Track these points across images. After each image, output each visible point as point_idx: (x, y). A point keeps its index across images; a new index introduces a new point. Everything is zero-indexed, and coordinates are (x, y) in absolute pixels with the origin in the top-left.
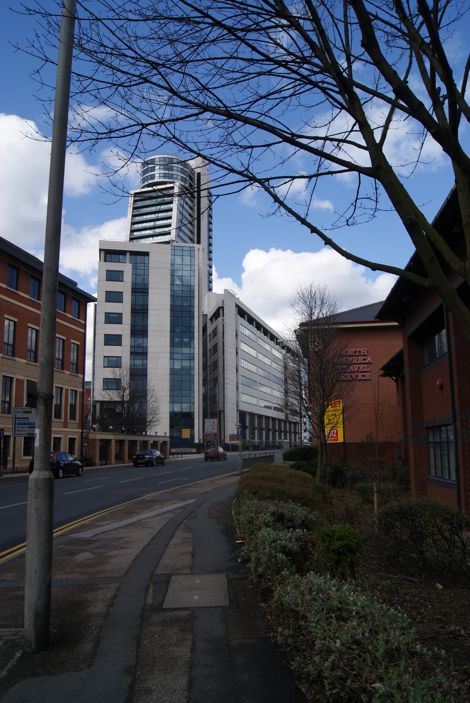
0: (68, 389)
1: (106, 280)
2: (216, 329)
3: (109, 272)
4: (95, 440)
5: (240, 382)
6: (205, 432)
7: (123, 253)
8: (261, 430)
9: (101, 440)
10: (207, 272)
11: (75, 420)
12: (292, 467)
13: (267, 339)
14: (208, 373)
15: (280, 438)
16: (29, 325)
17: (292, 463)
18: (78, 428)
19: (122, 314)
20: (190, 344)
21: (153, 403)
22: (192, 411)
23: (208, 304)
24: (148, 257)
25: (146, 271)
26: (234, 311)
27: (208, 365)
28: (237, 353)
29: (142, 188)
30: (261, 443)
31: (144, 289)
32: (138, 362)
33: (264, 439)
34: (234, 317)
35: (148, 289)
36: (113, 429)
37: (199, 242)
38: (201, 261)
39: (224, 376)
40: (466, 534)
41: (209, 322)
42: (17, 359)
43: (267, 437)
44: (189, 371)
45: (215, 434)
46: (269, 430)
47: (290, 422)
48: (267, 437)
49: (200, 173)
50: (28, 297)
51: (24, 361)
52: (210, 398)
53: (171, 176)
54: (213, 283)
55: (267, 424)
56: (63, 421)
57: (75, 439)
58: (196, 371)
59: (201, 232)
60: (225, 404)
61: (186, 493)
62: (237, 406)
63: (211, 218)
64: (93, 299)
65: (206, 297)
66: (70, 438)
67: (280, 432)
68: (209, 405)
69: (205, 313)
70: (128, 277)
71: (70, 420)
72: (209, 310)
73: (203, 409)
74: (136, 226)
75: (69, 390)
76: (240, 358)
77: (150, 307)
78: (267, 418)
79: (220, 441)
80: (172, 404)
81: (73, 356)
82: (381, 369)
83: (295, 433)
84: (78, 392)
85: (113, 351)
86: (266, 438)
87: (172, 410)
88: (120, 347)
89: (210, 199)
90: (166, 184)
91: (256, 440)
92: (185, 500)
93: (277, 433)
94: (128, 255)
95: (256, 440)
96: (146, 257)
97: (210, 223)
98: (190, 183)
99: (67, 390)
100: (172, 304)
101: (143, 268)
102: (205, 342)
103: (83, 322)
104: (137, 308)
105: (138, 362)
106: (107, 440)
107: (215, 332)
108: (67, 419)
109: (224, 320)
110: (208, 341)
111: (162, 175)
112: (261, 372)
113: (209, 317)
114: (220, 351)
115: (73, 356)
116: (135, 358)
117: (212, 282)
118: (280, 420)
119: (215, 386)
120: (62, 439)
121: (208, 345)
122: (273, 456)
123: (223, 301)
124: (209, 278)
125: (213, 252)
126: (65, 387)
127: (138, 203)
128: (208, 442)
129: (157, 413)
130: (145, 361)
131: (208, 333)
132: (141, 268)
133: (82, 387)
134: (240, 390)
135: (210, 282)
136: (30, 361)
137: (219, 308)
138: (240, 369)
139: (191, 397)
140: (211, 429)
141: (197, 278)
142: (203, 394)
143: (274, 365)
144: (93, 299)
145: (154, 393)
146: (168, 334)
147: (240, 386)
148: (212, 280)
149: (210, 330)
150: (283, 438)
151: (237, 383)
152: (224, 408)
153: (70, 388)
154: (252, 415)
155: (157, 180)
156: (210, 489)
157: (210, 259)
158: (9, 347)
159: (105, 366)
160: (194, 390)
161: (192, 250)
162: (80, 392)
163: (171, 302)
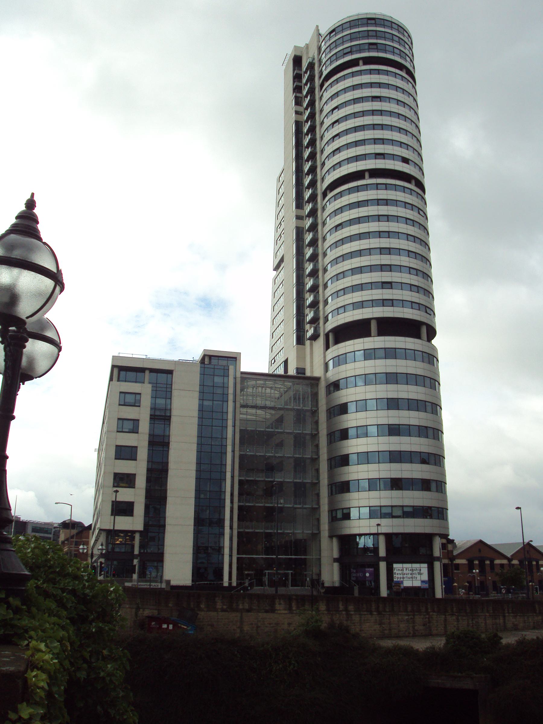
24: (171, 375)
25: (168, 393)
40: (541, 562)
70: (146, 401)
94: (147, 372)
96: (169, 376)
104: (158, 413)
132: (161, 386)
159: (120, 404)
160: (226, 465)
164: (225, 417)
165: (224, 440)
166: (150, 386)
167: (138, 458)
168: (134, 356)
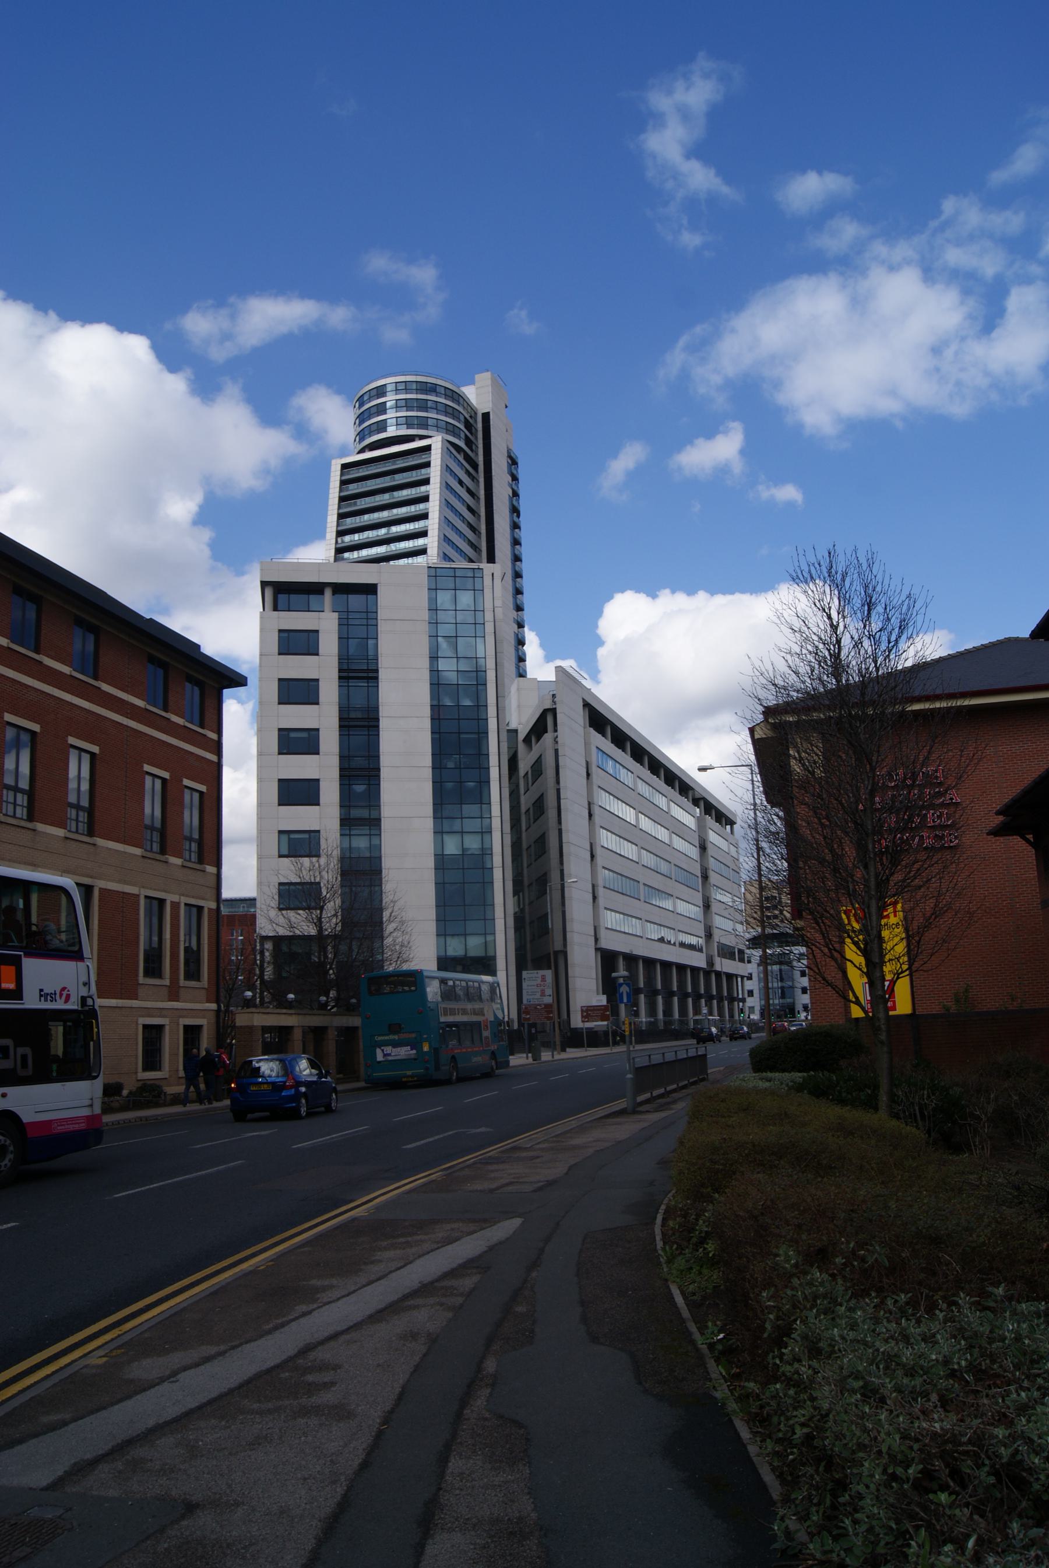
0: (179, 903)
1: (280, 654)
2: (538, 762)
3: (286, 635)
4: (250, 1029)
5: (600, 883)
6: (525, 1001)
7: (315, 589)
8: (652, 994)
9: (265, 1029)
10: (513, 635)
11: (198, 979)
12: (799, 1088)
13: (660, 783)
14: (525, 865)
15: (697, 1011)
16: (72, 740)
17: (798, 1076)
18: (208, 1001)
19: (318, 730)
20: (481, 796)
21: (395, 934)
22: (491, 953)
23: (519, 706)
26: (580, 717)
27: (525, 846)
28: (590, 815)
29: (360, 452)
30: (653, 1024)
31: (368, 671)
32: (361, 843)
33: (660, 1015)
34: (581, 730)
35: (377, 671)
36: (295, 1000)
37: (491, 559)
38: (498, 603)
39: (562, 871)
41: (521, 748)
42: (40, 827)
43: (668, 1012)
44: (480, 861)
45: (548, 1007)
46: (672, 994)
47: (718, 974)
48: (668, 1012)
49: (488, 413)
50: (66, 669)
51: (60, 832)
52: (531, 922)
53: (423, 423)
54: (527, 663)
55: (667, 980)
56: (167, 982)
57: (199, 1028)
58: (497, 860)
59: (496, 547)
60: (569, 935)
61: (487, 1185)
62: (596, 940)
63: (518, 516)
64: (237, 680)
65: (514, 689)
66: (145, 1027)
67: (697, 997)
68: (528, 939)
69: (513, 725)
70: (329, 644)
71: (185, 979)
72: (521, 718)
73: (516, 950)
74: (347, 539)
75: (182, 906)
76: (597, 828)
77: (383, 712)
78: (666, 965)
79: (559, 1023)
80: (442, 939)
81: (190, 818)
82: (998, 813)
83: (732, 999)
84: (206, 910)
85: (301, 818)
86: (665, 1014)
87: (443, 954)
88: (317, 807)
89: (515, 472)
90: (413, 440)
91: (643, 1018)
92: (485, 1222)
93: (690, 1000)
94: (328, 592)
95: (643, 1018)
97: (515, 526)
98: (466, 435)
99: (175, 906)
100: (435, 703)
101: (364, 622)
102: (514, 795)
103: (213, 736)
104: (353, 715)
105: (361, 843)
106: (348, 1029)
107: (537, 769)
108: (178, 979)
109: (559, 739)
110: (522, 790)
111: (403, 403)
112: (648, 859)
113: (521, 736)
114: (552, 813)
115: (190, 818)
116: (353, 832)
117: (524, 660)
118: (695, 970)
119: (543, 893)
120: (167, 1028)
121: (523, 799)
122: (705, 1055)
123: (554, 696)
124: (517, 650)
125: (525, 609)
126: (170, 898)
127: (351, 486)
128: (531, 1026)
129: (404, 956)
130: (375, 841)
131: (522, 773)
133: (214, 897)
134: (602, 901)
135: (521, 659)
136: (77, 832)
137: (545, 713)
138: (599, 851)
139: (488, 920)
140: (538, 995)
141: (490, 640)
142: (515, 914)
143: (679, 843)
144: (237, 680)
145: (396, 908)
146: (428, 773)
147: (601, 892)
148: (525, 654)
149: (524, 765)
150: (705, 1010)
151: (593, 886)
152: (565, 945)
153: (184, 900)
154: (631, 959)
155: (392, 431)
156: (559, 1170)
157: (519, 608)
158: (19, 796)
160: (493, 905)
161: (476, 575)
162: (210, 910)
163: (432, 699)
164: (478, 586)
165: (479, 614)
166: (336, 615)
167: (322, 801)
168: (300, 561)
